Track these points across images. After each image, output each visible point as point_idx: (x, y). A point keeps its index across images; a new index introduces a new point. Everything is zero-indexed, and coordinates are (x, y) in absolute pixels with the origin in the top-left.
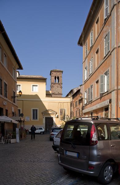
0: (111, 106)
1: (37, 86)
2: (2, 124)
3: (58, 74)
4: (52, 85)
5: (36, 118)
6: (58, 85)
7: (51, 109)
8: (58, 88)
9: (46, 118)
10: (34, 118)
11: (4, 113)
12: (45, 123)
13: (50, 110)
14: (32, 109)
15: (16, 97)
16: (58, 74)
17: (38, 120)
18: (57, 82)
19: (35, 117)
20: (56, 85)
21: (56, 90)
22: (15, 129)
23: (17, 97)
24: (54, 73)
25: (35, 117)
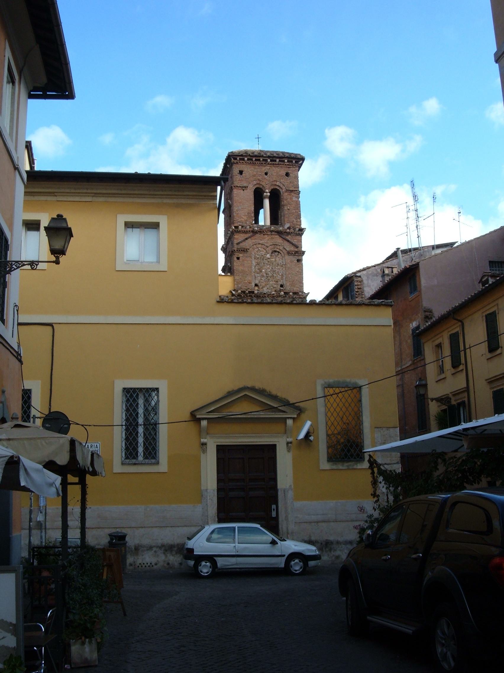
0: (122, 457)
1: (155, 226)
2: (498, 411)
3: (274, 175)
4: (239, 238)
5: (151, 453)
6: (278, 240)
7: (258, 385)
8: (279, 259)
9: (220, 449)
10: (130, 452)
11: (28, 190)
12: (215, 486)
13: (253, 389)
14: (120, 385)
15: (20, 264)
16: (274, 175)
17: (163, 466)
18: (261, 223)
19: (141, 449)
20: (266, 240)
21: (267, 269)
22: (29, 555)
23: (33, 264)
24: (249, 170)
25: (141, 449)
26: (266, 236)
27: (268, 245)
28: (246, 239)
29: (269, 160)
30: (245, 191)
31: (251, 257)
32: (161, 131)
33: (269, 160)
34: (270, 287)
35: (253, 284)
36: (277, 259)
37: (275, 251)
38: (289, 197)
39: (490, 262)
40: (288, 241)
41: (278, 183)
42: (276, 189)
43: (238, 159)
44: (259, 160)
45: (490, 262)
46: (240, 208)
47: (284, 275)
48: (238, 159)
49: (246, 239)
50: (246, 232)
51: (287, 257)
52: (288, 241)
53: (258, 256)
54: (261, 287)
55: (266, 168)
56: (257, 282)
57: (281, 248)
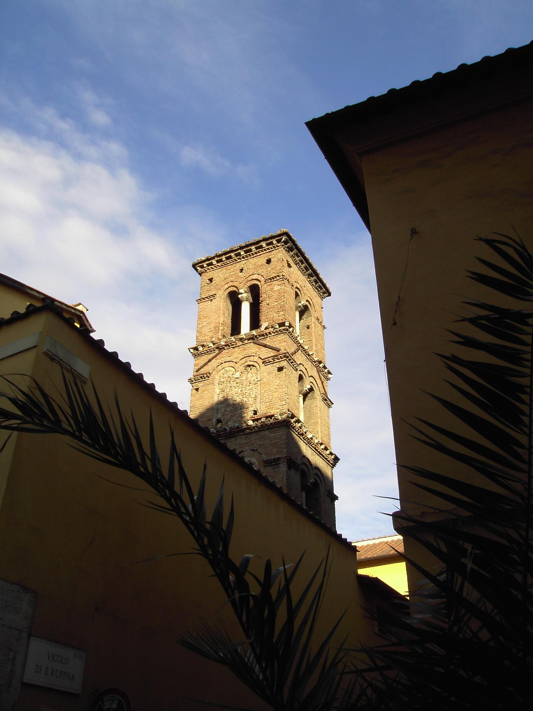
8: (252, 375)
26: (236, 349)
27: (238, 360)
28: (210, 361)
29: (242, 253)
30: (214, 301)
31: (213, 384)
32: (145, 289)
33: (242, 253)
34: (237, 418)
35: (214, 421)
36: (250, 375)
37: (249, 366)
38: (269, 287)
39: (329, 132)
40: (265, 346)
41: (255, 277)
42: (255, 284)
43: (205, 266)
44: (230, 257)
45: (329, 132)
46: (205, 324)
47: (259, 396)
48: (205, 266)
49: (210, 361)
50: (207, 353)
51: (263, 367)
52: (265, 346)
53: (222, 380)
54: (224, 422)
55: (242, 264)
56: (219, 416)
57: (256, 359)
